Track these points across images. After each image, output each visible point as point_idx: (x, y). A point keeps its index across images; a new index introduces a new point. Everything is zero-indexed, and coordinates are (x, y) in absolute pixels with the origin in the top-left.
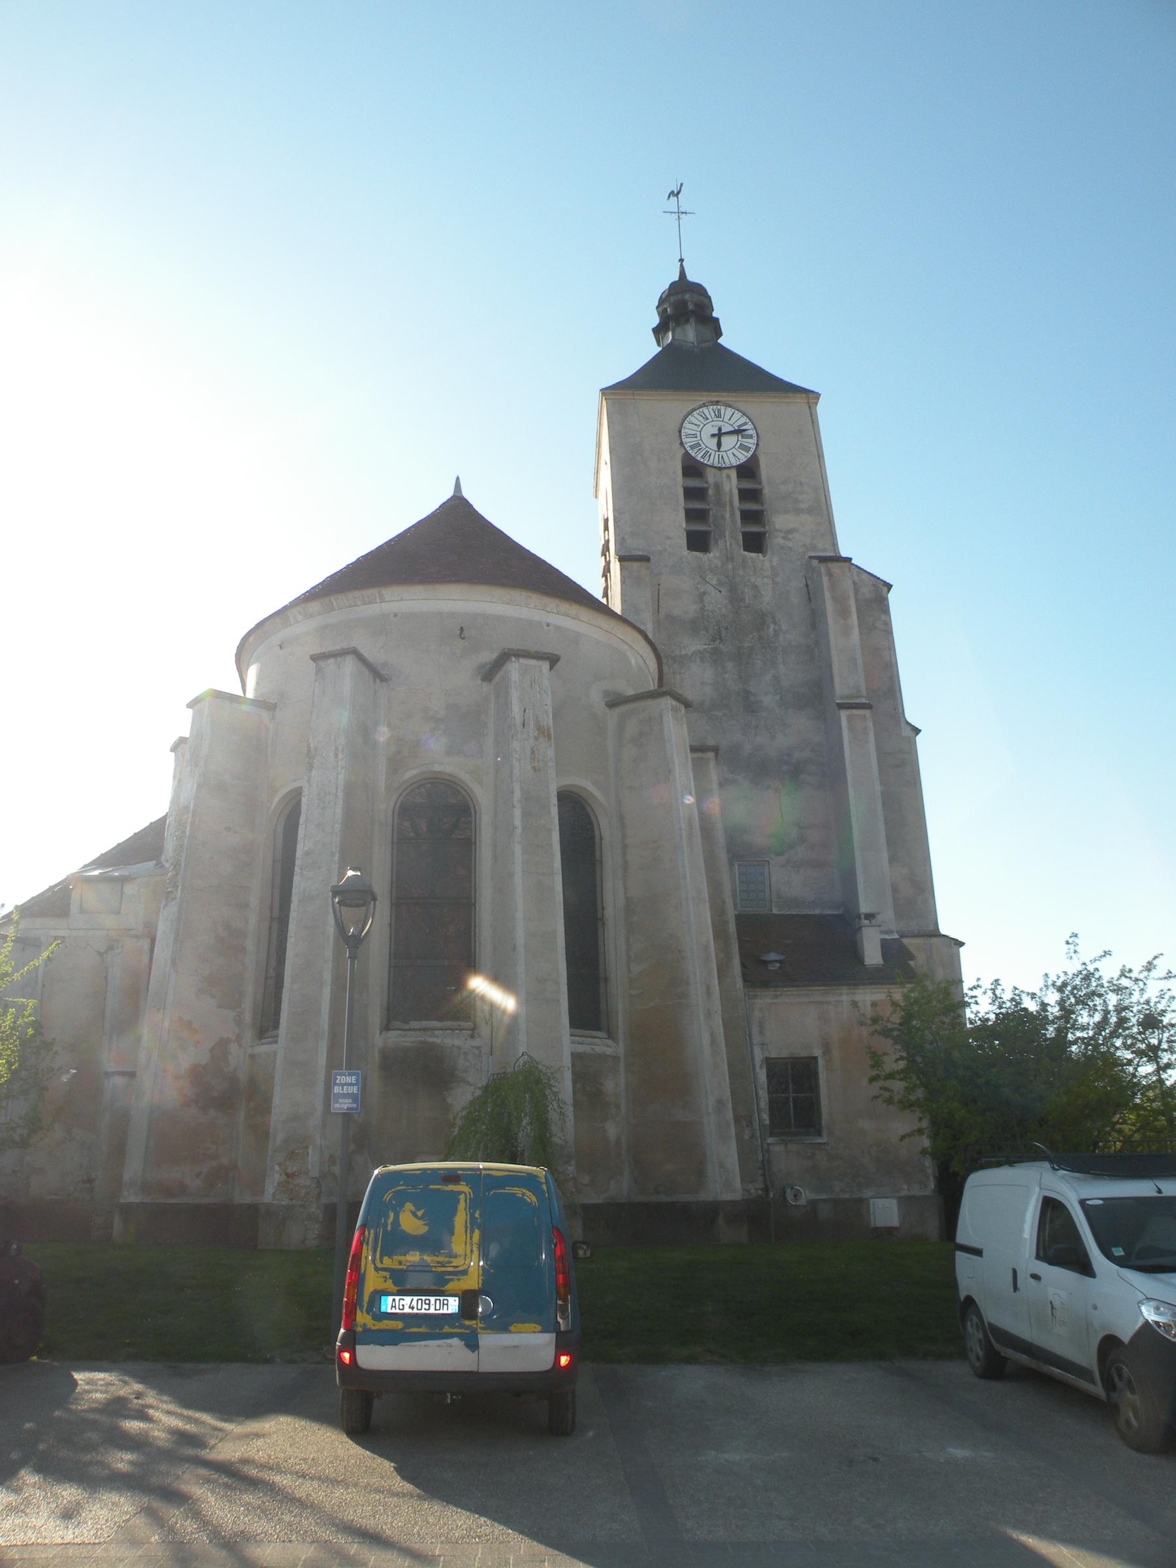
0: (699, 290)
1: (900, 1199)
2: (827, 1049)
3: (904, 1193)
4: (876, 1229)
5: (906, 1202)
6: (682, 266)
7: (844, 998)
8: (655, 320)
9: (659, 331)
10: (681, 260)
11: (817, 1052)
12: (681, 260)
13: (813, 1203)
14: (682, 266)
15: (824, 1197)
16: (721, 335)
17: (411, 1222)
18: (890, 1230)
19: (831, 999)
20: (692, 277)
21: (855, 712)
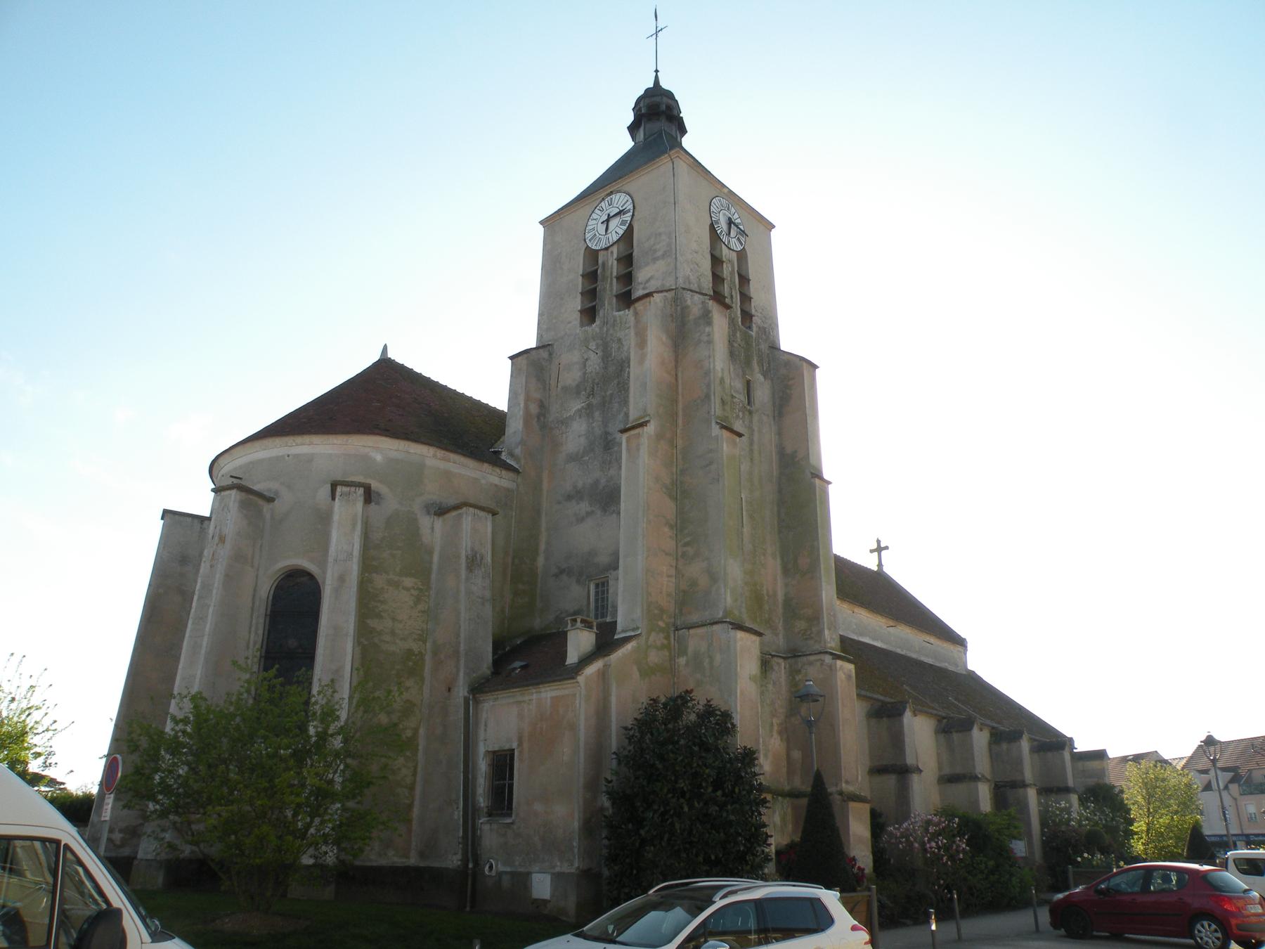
0: (669, 95)
1: (553, 874)
2: (520, 744)
3: (558, 869)
4: (536, 900)
5: (558, 878)
6: (657, 77)
7: (535, 696)
8: (630, 118)
9: (633, 129)
10: (657, 71)
11: (515, 745)
12: (657, 71)
13: (500, 874)
14: (657, 77)
15: (508, 869)
16: (683, 131)
17: (801, 625)
18: (545, 902)
19: (526, 698)
20: (665, 84)
21: (633, 432)
